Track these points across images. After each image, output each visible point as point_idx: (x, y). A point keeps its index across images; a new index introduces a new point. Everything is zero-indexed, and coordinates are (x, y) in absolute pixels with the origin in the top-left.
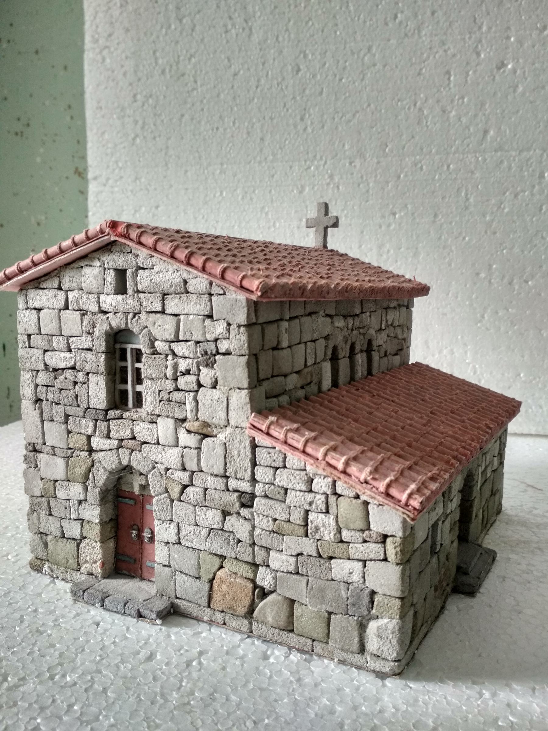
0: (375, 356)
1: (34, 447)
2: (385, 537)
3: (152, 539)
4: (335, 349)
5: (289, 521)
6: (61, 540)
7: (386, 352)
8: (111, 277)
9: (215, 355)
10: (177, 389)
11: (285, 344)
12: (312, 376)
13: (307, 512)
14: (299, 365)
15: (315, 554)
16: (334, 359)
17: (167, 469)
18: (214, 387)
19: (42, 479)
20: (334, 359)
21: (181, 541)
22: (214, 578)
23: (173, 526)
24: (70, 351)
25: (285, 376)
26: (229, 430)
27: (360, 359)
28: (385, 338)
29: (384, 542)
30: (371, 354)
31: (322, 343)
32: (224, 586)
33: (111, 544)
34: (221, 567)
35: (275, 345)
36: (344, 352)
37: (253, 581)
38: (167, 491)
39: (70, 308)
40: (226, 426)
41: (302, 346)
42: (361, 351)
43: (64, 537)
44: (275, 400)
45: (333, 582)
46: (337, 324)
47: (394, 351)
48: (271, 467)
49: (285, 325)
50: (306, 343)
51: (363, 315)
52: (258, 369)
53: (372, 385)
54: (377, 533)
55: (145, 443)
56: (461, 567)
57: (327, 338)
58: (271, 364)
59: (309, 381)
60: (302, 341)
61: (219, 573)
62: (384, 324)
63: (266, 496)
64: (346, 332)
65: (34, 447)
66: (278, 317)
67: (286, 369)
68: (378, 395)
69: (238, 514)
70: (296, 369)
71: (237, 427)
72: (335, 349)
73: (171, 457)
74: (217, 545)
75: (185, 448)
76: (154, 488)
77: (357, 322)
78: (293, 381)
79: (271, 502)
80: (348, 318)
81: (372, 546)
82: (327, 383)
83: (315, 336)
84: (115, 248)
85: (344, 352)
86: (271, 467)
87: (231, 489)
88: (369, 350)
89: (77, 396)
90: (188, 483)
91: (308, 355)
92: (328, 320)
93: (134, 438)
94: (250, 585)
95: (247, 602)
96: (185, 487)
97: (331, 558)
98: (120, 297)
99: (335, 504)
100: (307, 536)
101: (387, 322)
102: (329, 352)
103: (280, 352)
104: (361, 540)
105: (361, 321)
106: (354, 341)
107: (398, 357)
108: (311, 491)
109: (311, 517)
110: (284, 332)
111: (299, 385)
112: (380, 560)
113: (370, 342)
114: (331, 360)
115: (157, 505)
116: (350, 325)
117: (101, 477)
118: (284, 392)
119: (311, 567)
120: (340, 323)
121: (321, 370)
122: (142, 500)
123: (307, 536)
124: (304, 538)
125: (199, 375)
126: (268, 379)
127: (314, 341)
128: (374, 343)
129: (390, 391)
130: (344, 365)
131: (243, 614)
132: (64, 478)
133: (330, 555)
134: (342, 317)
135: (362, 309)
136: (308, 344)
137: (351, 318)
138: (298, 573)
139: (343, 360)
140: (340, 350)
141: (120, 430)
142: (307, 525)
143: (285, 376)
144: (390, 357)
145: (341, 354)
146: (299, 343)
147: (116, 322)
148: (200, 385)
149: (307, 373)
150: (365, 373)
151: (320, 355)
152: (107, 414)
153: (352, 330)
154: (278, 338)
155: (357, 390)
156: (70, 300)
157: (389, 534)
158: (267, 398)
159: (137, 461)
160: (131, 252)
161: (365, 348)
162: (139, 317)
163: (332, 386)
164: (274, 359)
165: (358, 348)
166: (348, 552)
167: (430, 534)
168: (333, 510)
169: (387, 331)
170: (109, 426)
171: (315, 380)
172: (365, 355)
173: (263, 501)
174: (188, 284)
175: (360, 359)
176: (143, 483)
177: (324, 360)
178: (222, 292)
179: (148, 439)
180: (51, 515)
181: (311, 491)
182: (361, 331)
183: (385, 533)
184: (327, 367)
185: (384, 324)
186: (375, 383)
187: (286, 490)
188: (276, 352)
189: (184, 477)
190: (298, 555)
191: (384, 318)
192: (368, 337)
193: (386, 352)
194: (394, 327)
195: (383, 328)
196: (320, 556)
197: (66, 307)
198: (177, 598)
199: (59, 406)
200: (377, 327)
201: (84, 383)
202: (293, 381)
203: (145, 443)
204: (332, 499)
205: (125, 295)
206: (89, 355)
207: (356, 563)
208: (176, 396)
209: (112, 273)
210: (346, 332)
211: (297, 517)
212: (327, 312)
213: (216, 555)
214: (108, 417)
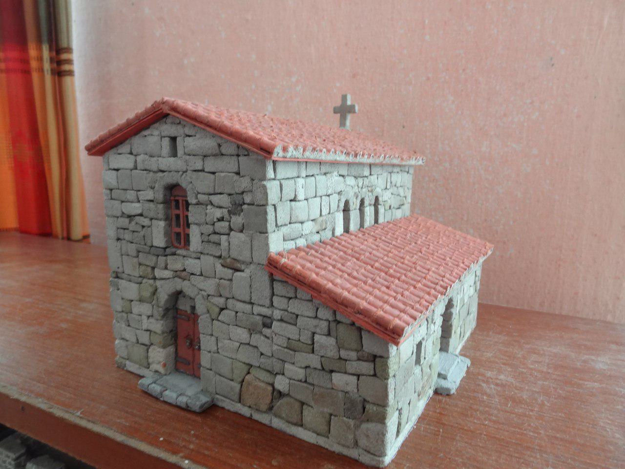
0: (381, 210)
1: (117, 275)
2: (375, 357)
3: (199, 349)
4: (347, 203)
5: (299, 340)
6: (136, 345)
7: (390, 207)
8: (166, 142)
9: (241, 205)
10: (215, 233)
11: (301, 196)
12: (326, 223)
13: (314, 334)
14: (315, 214)
15: (319, 367)
16: (346, 210)
17: (209, 295)
18: (241, 231)
19: (123, 299)
20: (346, 210)
21: (219, 350)
22: (243, 381)
23: (213, 338)
24: (139, 201)
25: (302, 223)
26: (252, 266)
27: (369, 211)
28: (390, 195)
29: (374, 361)
30: (378, 207)
31: (335, 197)
32: (251, 388)
33: (171, 349)
34: (249, 373)
35: (292, 197)
36: (355, 205)
37: (272, 385)
38: (208, 312)
39: (138, 168)
40: (251, 263)
41: (318, 199)
42: (370, 205)
43: (138, 343)
44: (293, 242)
45: (333, 391)
46: (348, 183)
47: (396, 206)
48: (285, 297)
49: (301, 181)
50: (321, 197)
51: (372, 177)
52: (276, 217)
53: (377, 232)
54: (368, 353)
55: (192, 274)
56: (442, 374)
57: (340, 193)
58: (289, 213)
59: (324, 228)
60: (318, 195)
61: (247, 377)
62: (389, 184)
63: (281, 320)
64: (356, 189)
65: (117, 275)
66: (295, 175)
67: (302, 216)
68: (380, 239)
69: (261, 333)
70: (312, 218)
71: (259, 264)
72: (347, 203)
73: (209, 286)
74: (246, 355)
75: (221, 279)
76: (200, 308)
77: (366, 181)
78: (309, 227)
79: (284, 325)
80: (359, 179)
81: (365, 364)
82: (340, 230)
83: (329, 192)
84: (169, 120)
85: (355, 205)
86: (285, 297)
87: (255, 313)
88: (376, 203)
89: (144, 236)
90: (224, 307)
91: (323, 207)
92: (341, 178)
93: (184, 270)
94: (270, 388)
95: (268, 401)
96: (222, 309)
97: (332, 371)
98: (172, 159)
99: (335, 328)
100: (313, 352)
101: (391, 183)
102: (342, 205)
103: (297, 203)
104: (356, 358)
105: (370, 182)
106: (363, 196)
107: (400, 210)
108: (316, 317)
109: (317, 337)
110: (301, 187)
111: (315, 231)
112: (370, 376)
113: (377, 199)
114: (344, 211)
115: (203, 321)
116: (360, 185)
117: (163, 296)
118: (301, 236)
119: (317, 378)
120: (351, 181)
121: (334, 219)
122: (193, 317)
123: (313, 352)
124: (311, 355)
125: (230, 221)
126: (286, 225)
127: (329, 196)
128: (380, 199)
129: (391, 236)
130: (354, 215)
131: (264, 410)
132: (138, 298)
133: (331, 369)
134: (353, 178)
135: (371, 172)
136: (323, 198)
137: (361, 179)
138: (306, 382)
139: (354, 211)
140: (351, 203)
141: (176, 264)
142: (313, 344)
143: (302, 223)
144: (394, 210)
145: (352, 207)
146: (315, 197)
147: (170, 179)
148: (231, 229)
149: (322, 221)
150: (373, 222)
151: (334, 206)
152: (165, 251)
153: (362, 188)
154: (295, 192)
155: (364, 235)
156: (138, 162)
157: (378, 355)
158: (284, 240)
159: (186, 287)
160: (180, 123)
161: (373, 202)
162: (186, 175)
163: (375, 223)
164: (291, 209)
165: (367, 203)
166: (345, 368)
167: (415, 351)
168: (333, 333)
169: (391, 191)
170: (166, 261)
171: (329, 227)
172: (373, 208)
173: (278, 324)
174: (222, 147)
175: (369, 211)
176: (193, 304)
177: (338, 211)
178: (246, 153)
179: (195, 271)
180: (129, 326)
181: (316, 317)
182: (370, 189)
183: (375, 354)
184: (340, 217)
185: (389, 184)
186: (380, 230)
187: (297, 316)
188: (293, 203)
189: (221, 301)
190: (306, 367)
191: (389, 180)
192: (375, 194)
193: (390, 207)
194: (398, 187)
195: (388, 187)
196: (323, 369)
197: (136, 168)
198: (217, 394)
199: (133, 244)
200: (383, 187)
201: (149, 227)
202: (309, 227)
203: (192, 274)
204: (333, 325)
205: (176, 158)
206: (151, 205)
207: (351, 377)
208: (214, 238)
209: (167, 139)
210: (356, 189)
211: (305, 338)
212: (341, 173)
213: (244, 363)
214: (166, 253)
